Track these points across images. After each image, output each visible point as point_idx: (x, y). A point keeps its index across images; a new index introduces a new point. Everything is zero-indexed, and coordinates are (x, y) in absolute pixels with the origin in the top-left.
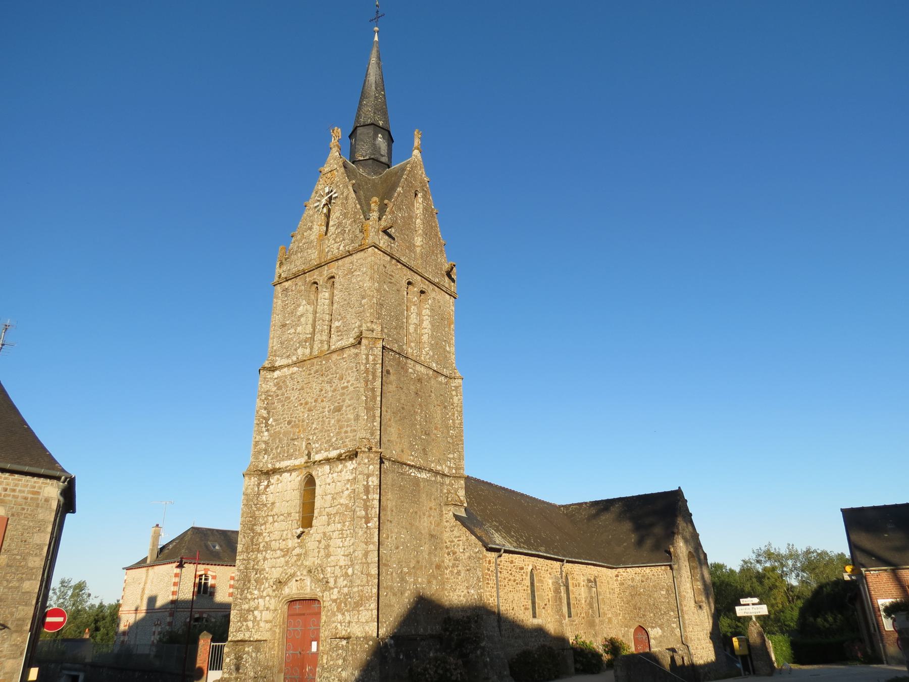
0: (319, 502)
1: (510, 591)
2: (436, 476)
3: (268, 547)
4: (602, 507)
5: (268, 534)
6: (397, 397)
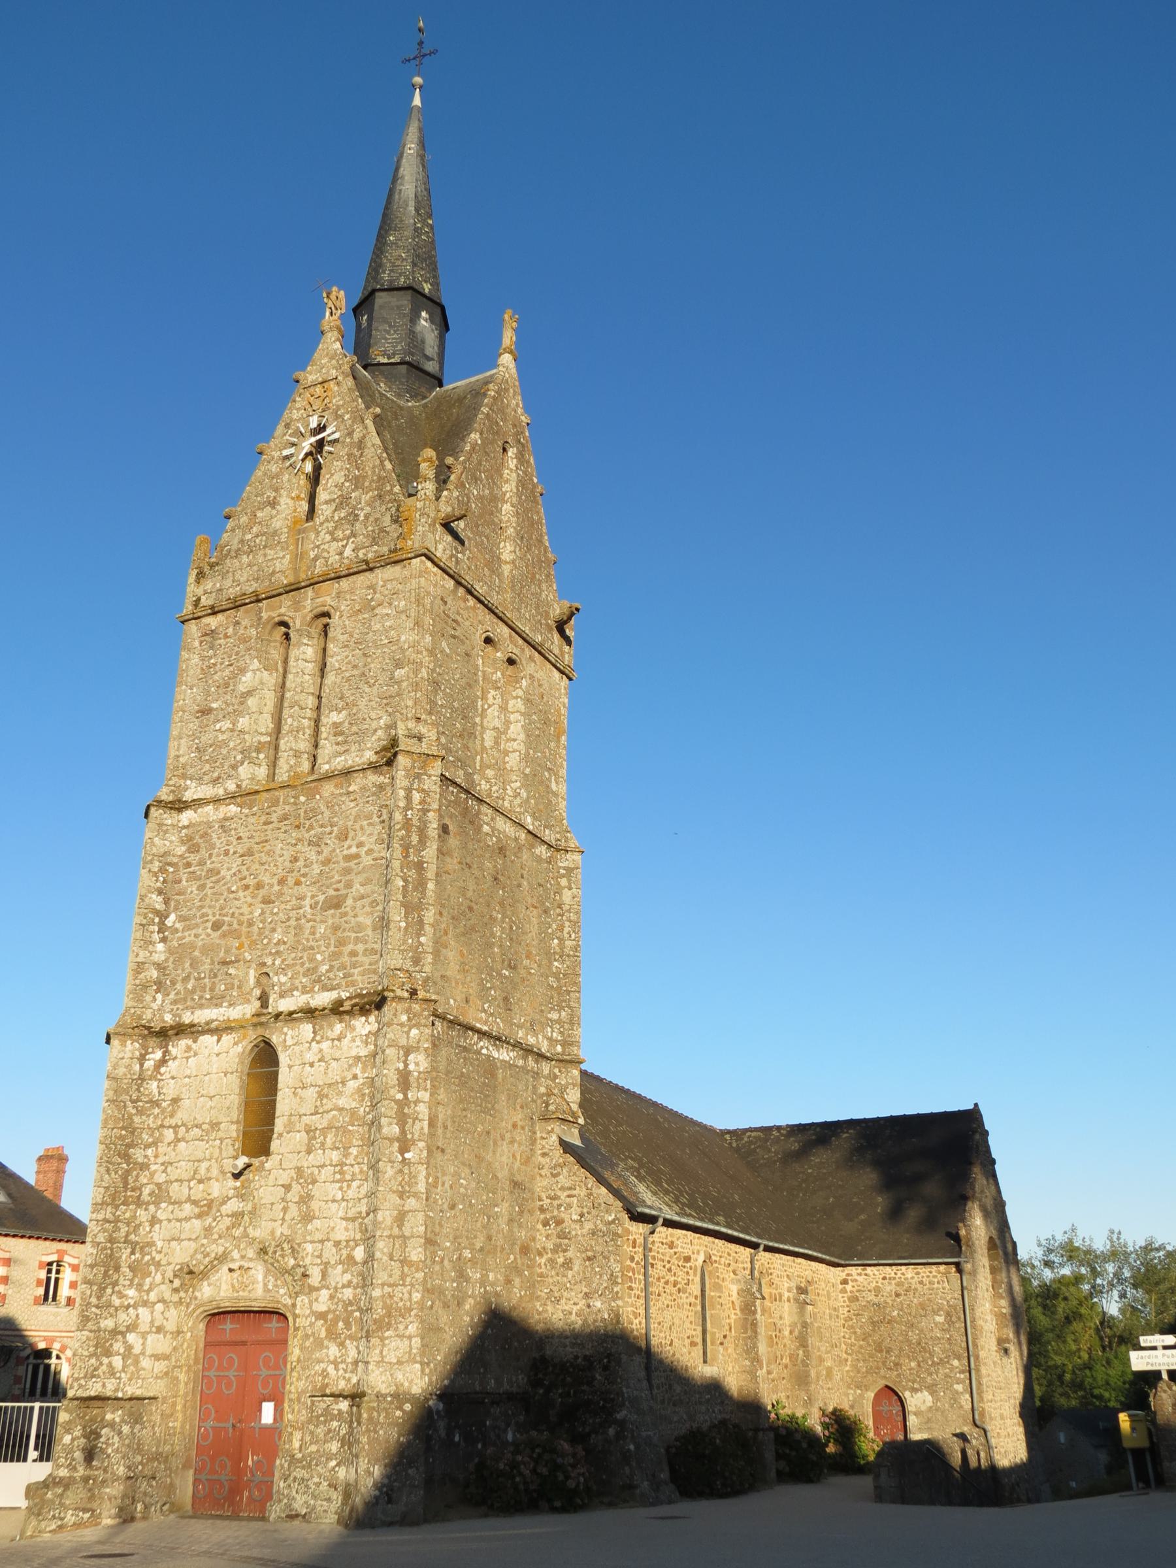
0: (286, 1101)
1: (668, 1306)
2: (525, 1058)
3: (161, 1195)
4: (814, 1137)
5: (163, 1167)
6: (460, 884)
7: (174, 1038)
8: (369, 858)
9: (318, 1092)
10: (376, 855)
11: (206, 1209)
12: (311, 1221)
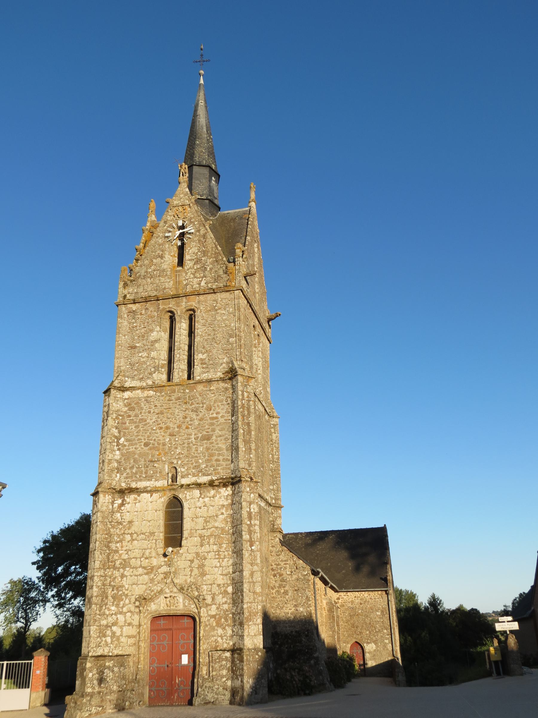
0: (189, 524)
5: (126, 552)
7: (127, 494)
8: (223, 419)
9: (204, 520)
10: (226, 418)
11: (150, 570)
12: (205, 576)
